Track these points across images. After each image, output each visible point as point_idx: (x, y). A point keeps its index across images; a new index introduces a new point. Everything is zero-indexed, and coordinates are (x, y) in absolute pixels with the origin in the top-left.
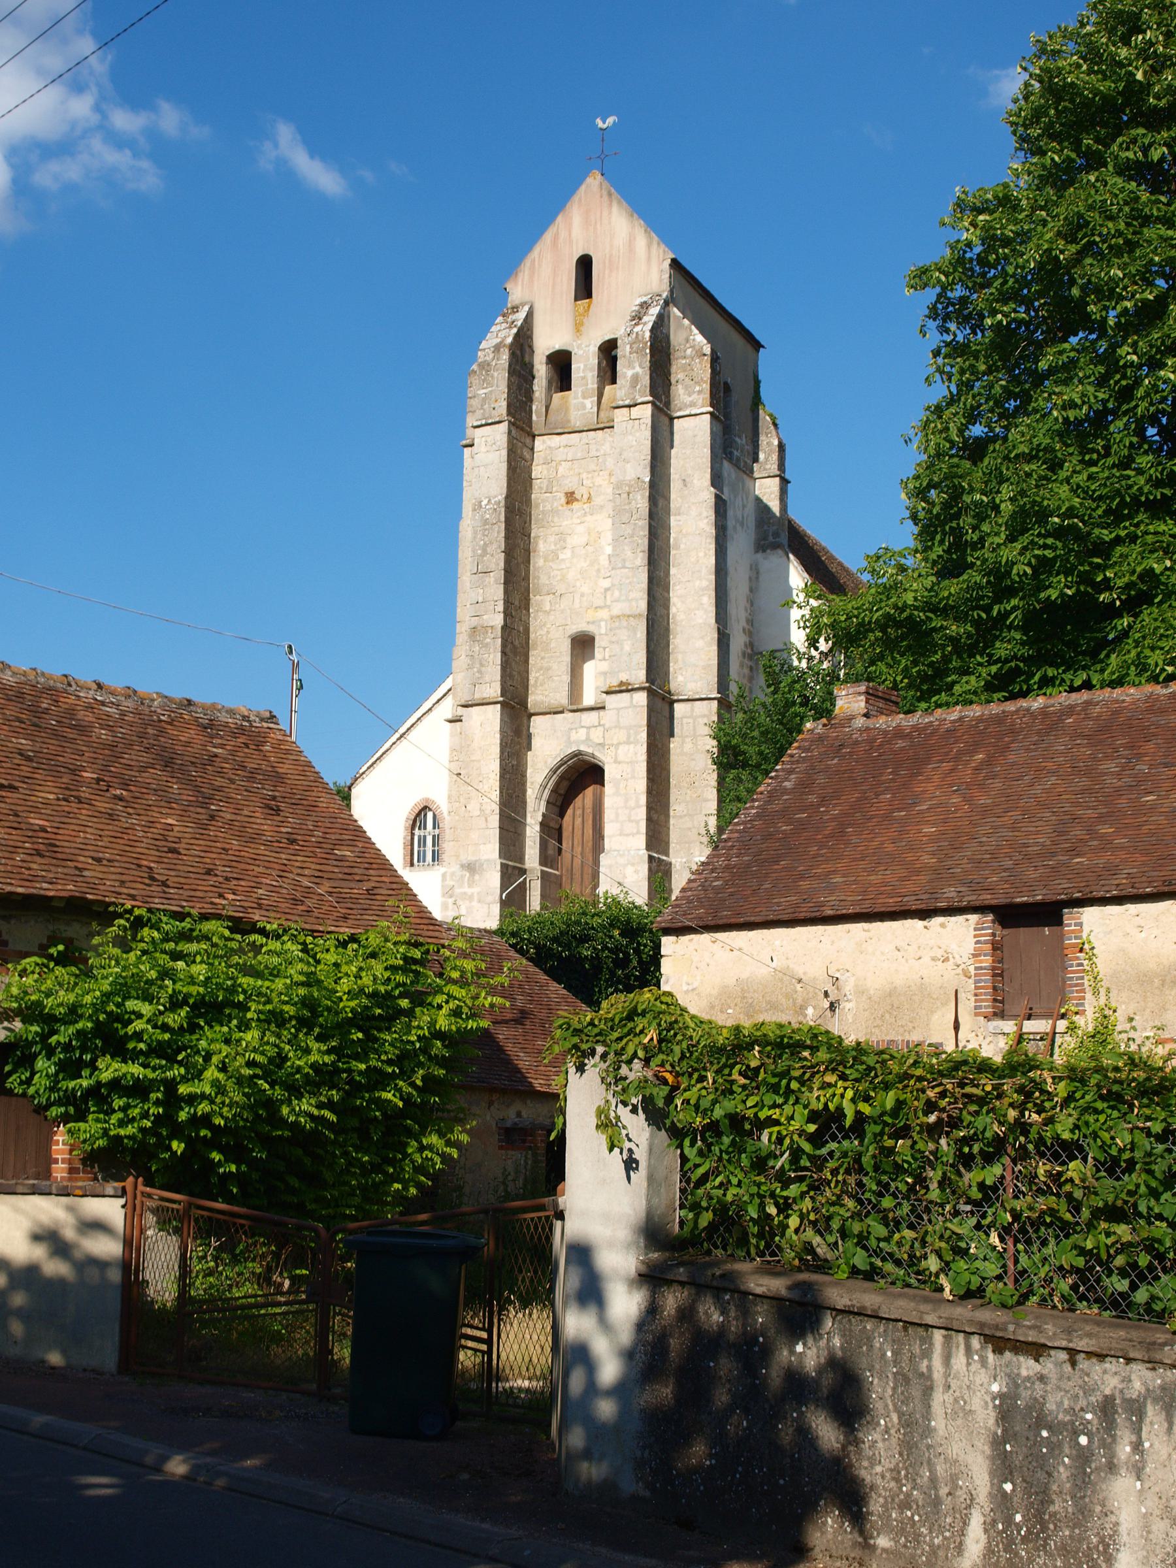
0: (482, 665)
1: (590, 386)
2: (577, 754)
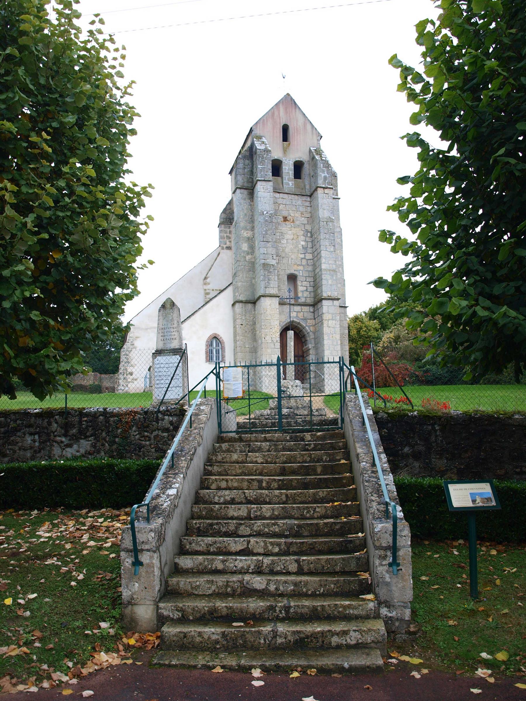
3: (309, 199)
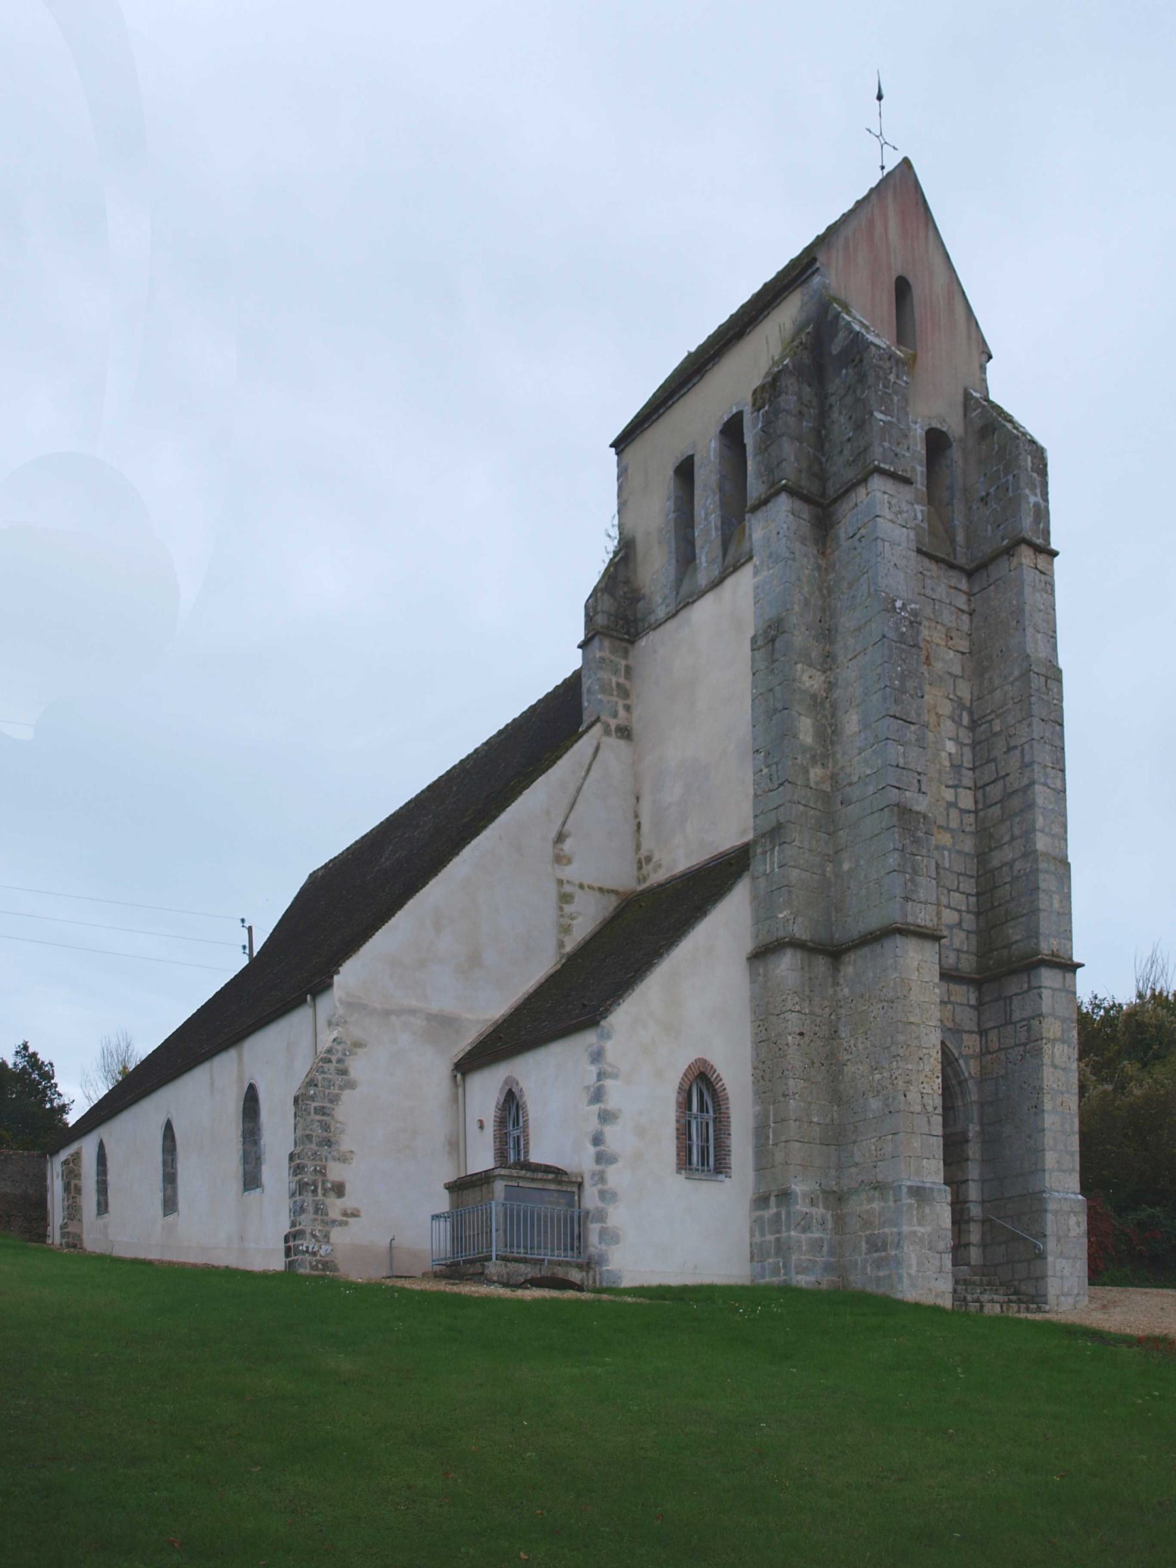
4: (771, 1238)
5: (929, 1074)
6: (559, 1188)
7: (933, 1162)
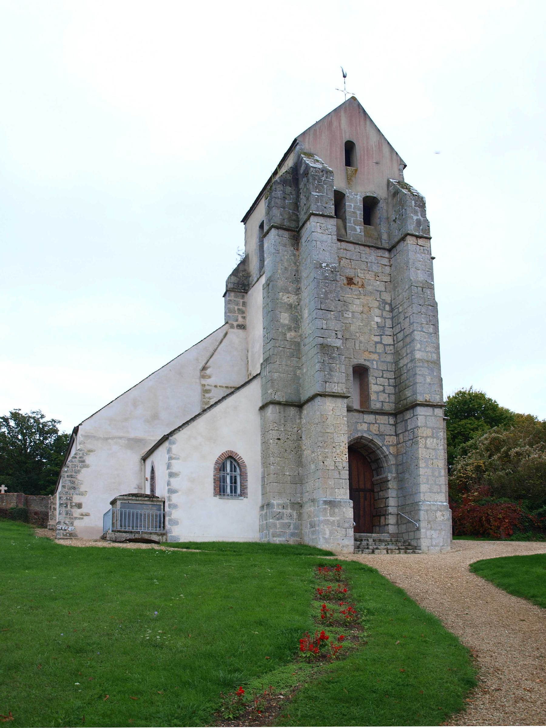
0: (331, 370)
1: (358, 219)
2: (362, 437)
3: (387, 254)
4: (265, 522)
5: (339, 453)
6: (152, 503)
7: (342, 491)
